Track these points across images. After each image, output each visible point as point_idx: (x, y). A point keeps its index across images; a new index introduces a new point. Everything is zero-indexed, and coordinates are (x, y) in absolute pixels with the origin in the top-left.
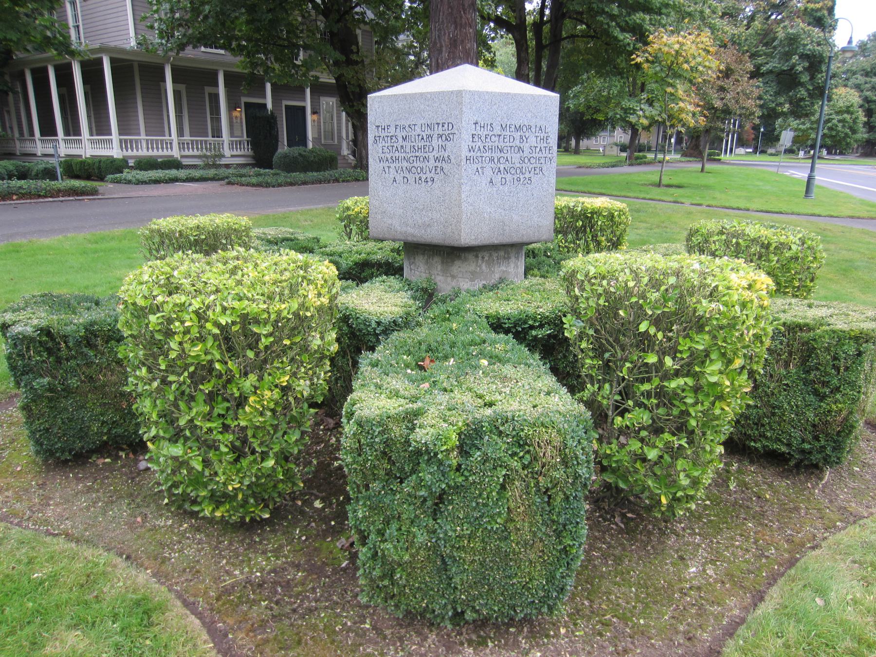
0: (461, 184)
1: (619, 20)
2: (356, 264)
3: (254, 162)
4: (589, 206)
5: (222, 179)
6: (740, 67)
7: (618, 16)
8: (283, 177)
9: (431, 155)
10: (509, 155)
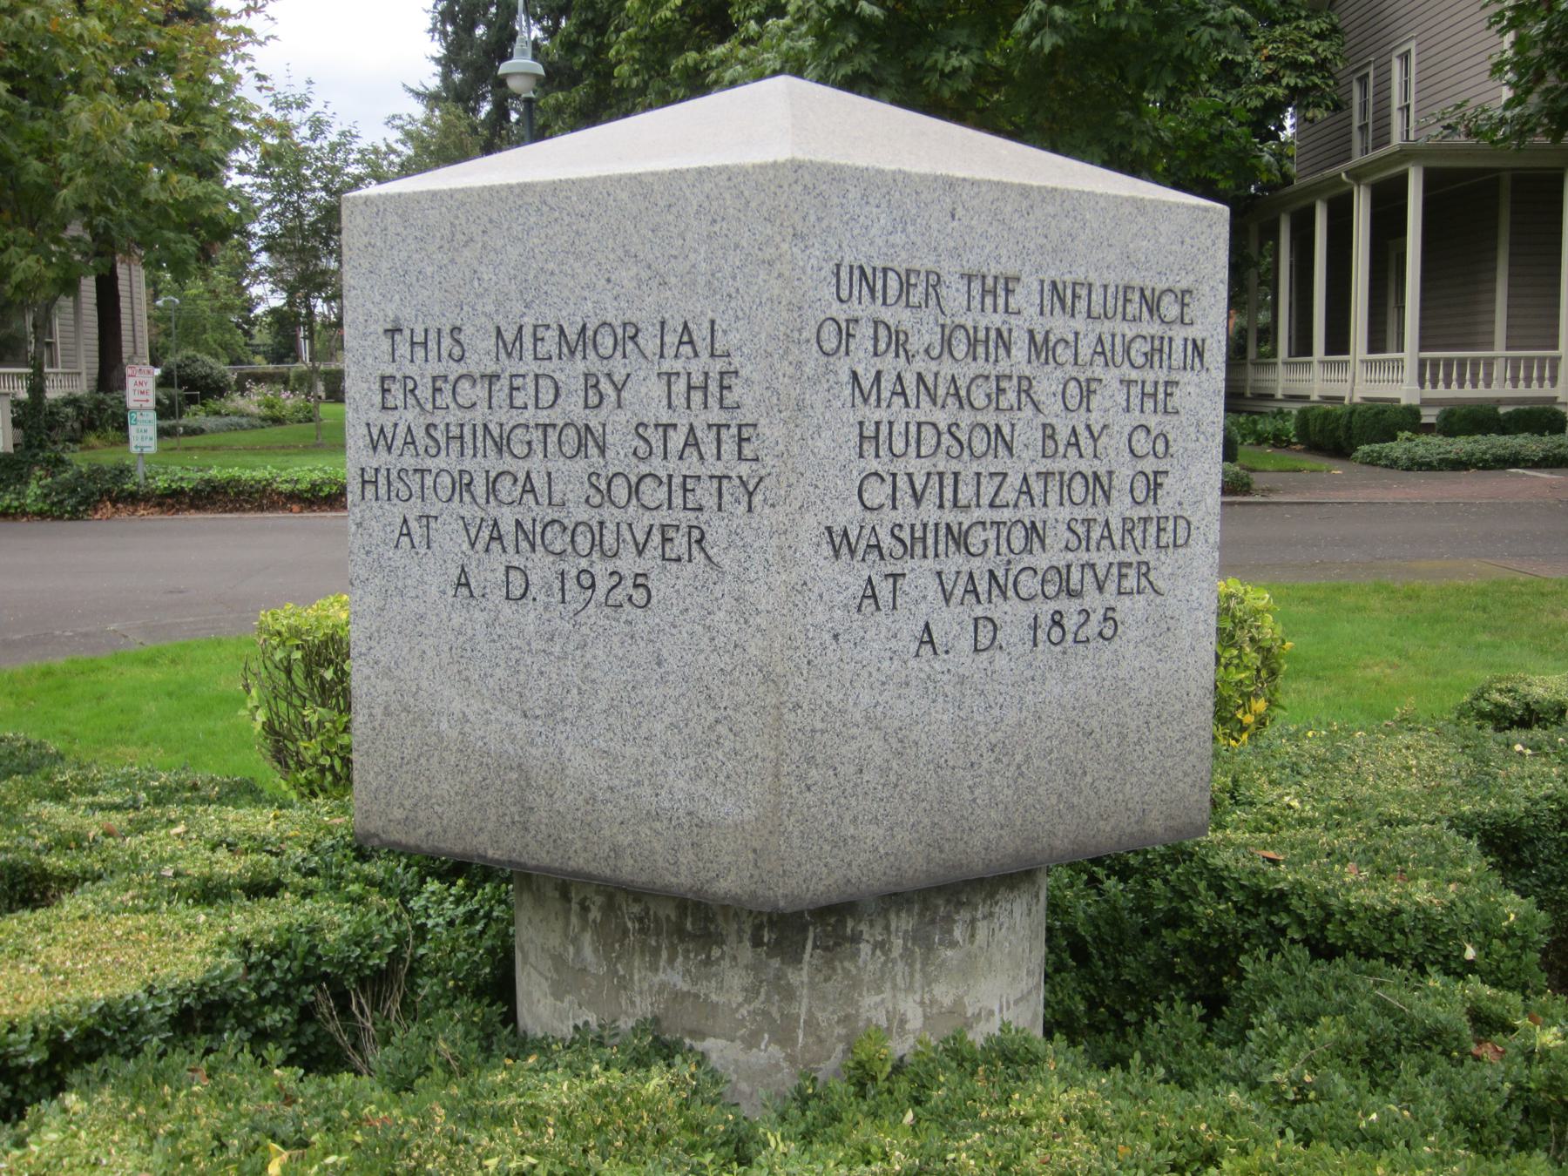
10: (536, 464)
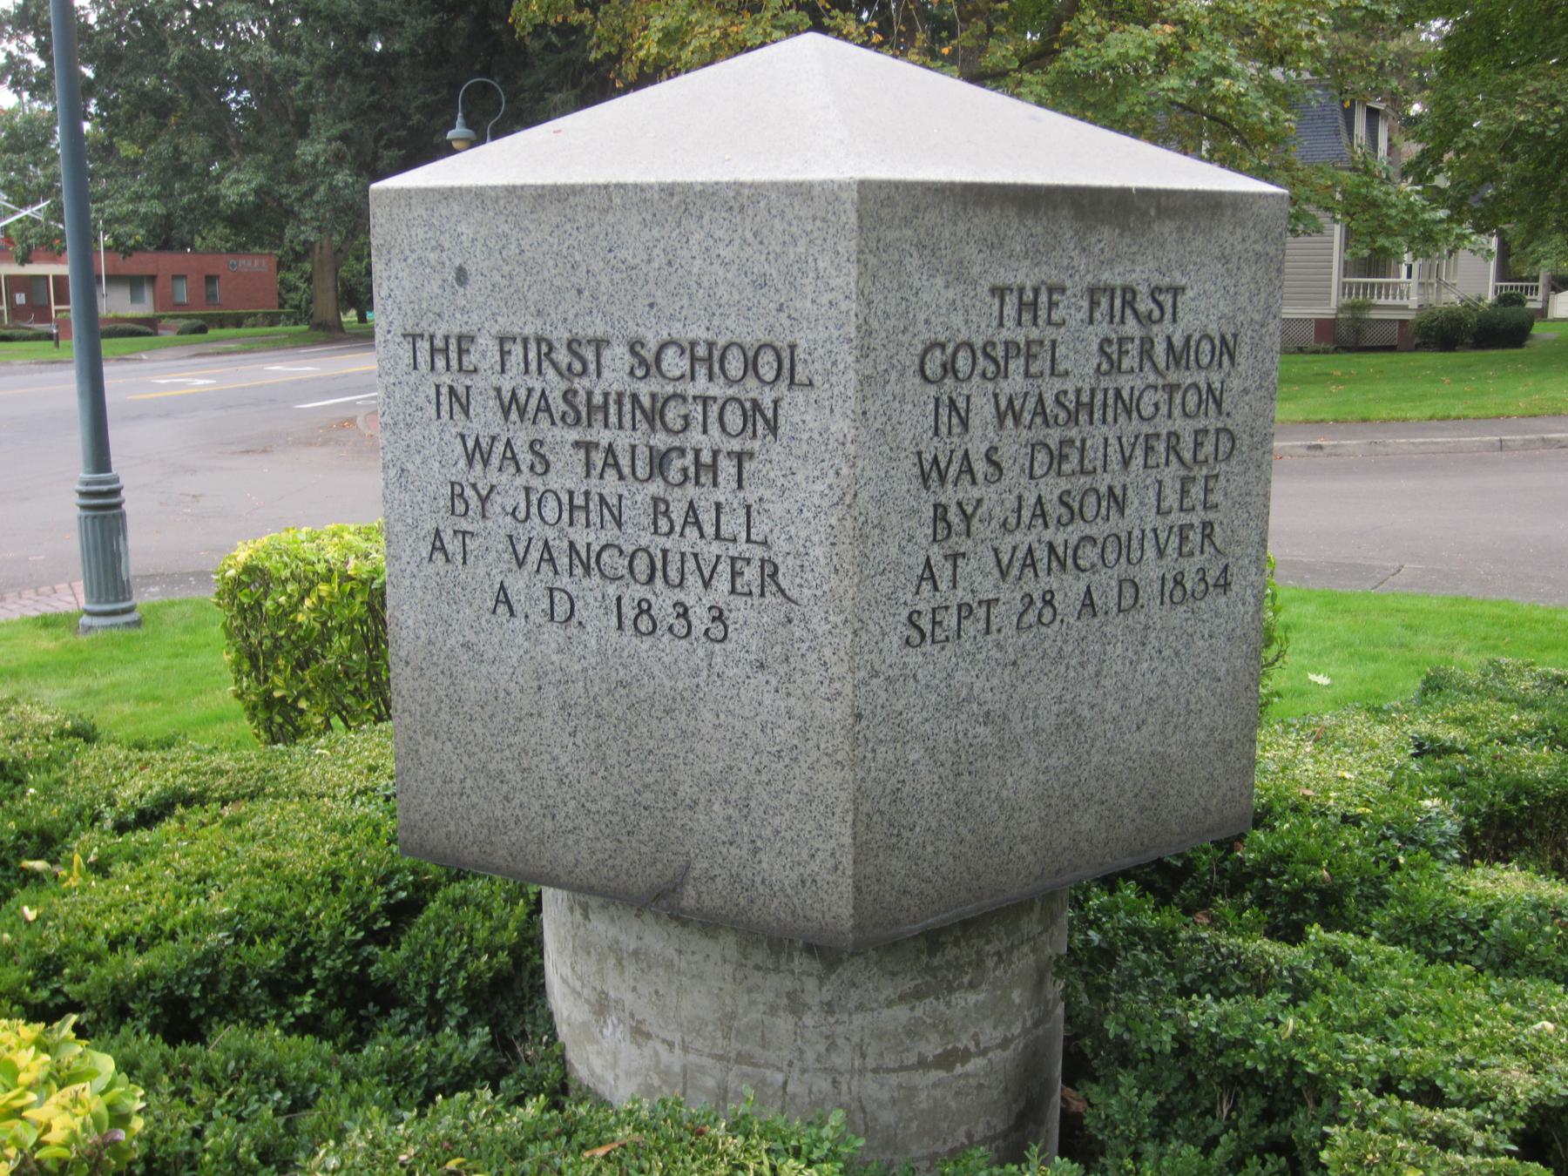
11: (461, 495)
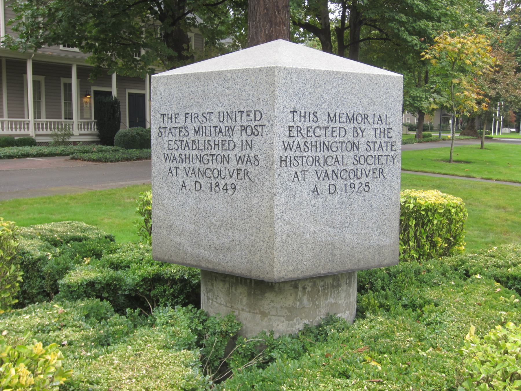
0: (272, 196)
1: (407, 26)
2: (144, 279)
3: (99, 140)
4: (422, 202)
5: (68, 155)
6: (508, 63)
7: (406, 22)
8: (122, 152)
9: (232, 154)
10: (339, 154)
11: (356, 131)
